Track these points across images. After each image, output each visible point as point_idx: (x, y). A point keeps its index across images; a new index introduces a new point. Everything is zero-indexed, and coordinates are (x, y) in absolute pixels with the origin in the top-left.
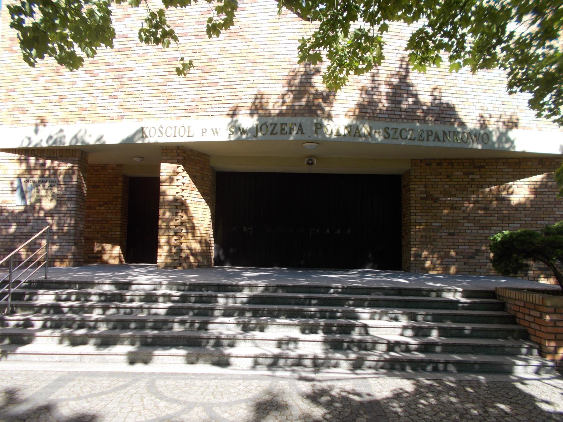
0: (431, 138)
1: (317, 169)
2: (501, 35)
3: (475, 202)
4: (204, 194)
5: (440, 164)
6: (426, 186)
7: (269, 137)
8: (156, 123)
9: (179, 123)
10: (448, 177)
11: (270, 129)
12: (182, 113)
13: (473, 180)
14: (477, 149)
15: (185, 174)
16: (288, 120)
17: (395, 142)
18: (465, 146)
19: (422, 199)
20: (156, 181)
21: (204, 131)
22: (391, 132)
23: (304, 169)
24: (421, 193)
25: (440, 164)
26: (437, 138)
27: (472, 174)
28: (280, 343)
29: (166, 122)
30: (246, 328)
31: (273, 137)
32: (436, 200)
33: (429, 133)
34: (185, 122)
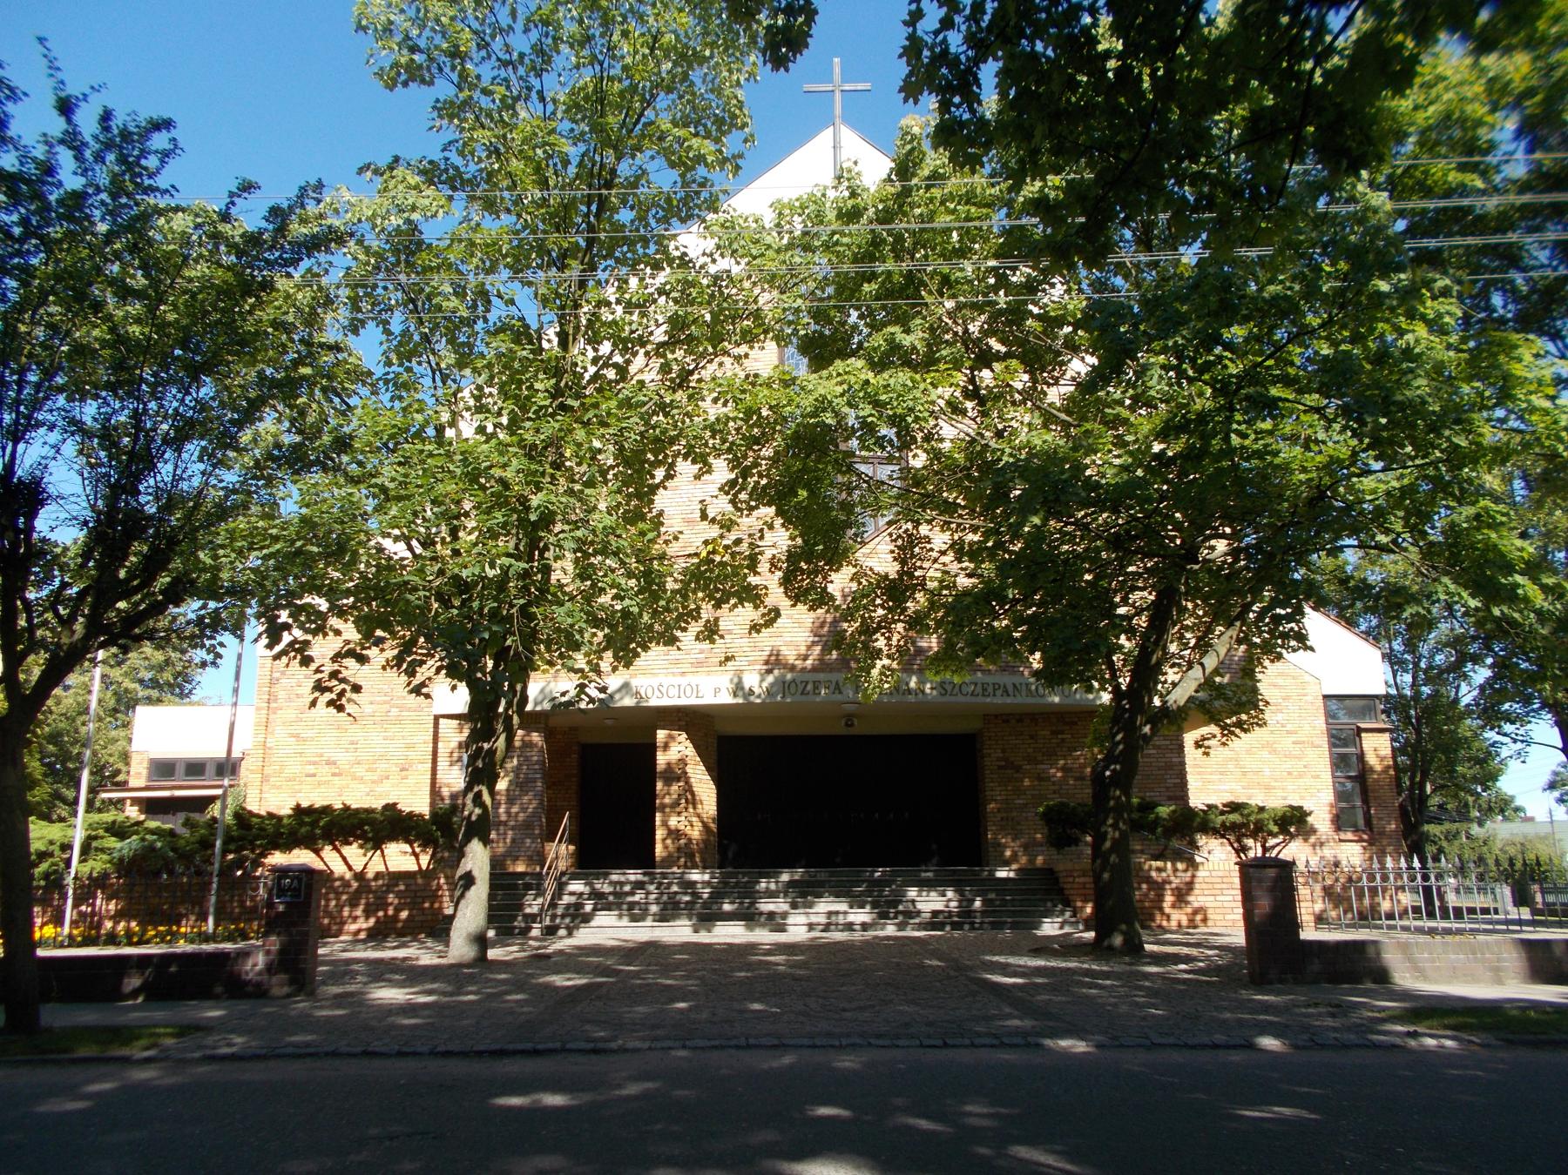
0: (999, 693)
1: (859, 729)
2: (1248, 398)
3: (1063, 769)
4: (709, 769)
5: (1020, 720)
6: (1004, 751)
7: (799, 698)
8: (655, 682)
9: (683, 681)
10: (1032, 737)
11: (801, 687)
12: (686, 668)
13: (1063, 740)
14: (1053, 705)
15: (688, 743)
16: (821, 676)
17: (953, 699)
18: (1041, 701)
19: (1000, 767)
20: (651, 748)
21: (717, 691)
22: (949, 688)
23: (840, 729)
24: (998, 759)
25: (1020, 720)
26: (1006, 692)
27: (1062, 732)
28: (830, 914)
29: (666, 681)
30: (794, 906)
31: (804, 698)
32: (1018, 769)
33: (996, 686)
34: (692, 679)
